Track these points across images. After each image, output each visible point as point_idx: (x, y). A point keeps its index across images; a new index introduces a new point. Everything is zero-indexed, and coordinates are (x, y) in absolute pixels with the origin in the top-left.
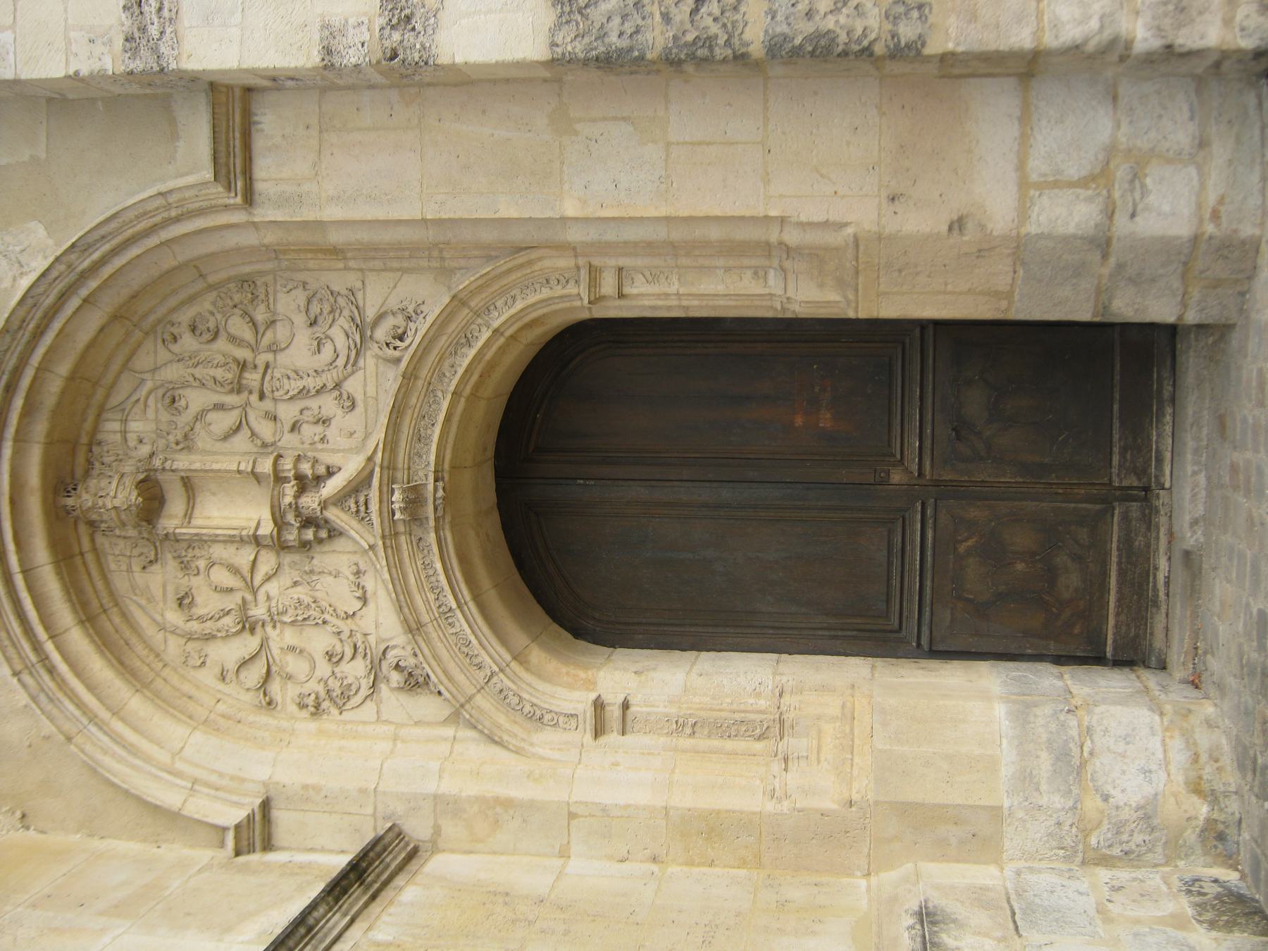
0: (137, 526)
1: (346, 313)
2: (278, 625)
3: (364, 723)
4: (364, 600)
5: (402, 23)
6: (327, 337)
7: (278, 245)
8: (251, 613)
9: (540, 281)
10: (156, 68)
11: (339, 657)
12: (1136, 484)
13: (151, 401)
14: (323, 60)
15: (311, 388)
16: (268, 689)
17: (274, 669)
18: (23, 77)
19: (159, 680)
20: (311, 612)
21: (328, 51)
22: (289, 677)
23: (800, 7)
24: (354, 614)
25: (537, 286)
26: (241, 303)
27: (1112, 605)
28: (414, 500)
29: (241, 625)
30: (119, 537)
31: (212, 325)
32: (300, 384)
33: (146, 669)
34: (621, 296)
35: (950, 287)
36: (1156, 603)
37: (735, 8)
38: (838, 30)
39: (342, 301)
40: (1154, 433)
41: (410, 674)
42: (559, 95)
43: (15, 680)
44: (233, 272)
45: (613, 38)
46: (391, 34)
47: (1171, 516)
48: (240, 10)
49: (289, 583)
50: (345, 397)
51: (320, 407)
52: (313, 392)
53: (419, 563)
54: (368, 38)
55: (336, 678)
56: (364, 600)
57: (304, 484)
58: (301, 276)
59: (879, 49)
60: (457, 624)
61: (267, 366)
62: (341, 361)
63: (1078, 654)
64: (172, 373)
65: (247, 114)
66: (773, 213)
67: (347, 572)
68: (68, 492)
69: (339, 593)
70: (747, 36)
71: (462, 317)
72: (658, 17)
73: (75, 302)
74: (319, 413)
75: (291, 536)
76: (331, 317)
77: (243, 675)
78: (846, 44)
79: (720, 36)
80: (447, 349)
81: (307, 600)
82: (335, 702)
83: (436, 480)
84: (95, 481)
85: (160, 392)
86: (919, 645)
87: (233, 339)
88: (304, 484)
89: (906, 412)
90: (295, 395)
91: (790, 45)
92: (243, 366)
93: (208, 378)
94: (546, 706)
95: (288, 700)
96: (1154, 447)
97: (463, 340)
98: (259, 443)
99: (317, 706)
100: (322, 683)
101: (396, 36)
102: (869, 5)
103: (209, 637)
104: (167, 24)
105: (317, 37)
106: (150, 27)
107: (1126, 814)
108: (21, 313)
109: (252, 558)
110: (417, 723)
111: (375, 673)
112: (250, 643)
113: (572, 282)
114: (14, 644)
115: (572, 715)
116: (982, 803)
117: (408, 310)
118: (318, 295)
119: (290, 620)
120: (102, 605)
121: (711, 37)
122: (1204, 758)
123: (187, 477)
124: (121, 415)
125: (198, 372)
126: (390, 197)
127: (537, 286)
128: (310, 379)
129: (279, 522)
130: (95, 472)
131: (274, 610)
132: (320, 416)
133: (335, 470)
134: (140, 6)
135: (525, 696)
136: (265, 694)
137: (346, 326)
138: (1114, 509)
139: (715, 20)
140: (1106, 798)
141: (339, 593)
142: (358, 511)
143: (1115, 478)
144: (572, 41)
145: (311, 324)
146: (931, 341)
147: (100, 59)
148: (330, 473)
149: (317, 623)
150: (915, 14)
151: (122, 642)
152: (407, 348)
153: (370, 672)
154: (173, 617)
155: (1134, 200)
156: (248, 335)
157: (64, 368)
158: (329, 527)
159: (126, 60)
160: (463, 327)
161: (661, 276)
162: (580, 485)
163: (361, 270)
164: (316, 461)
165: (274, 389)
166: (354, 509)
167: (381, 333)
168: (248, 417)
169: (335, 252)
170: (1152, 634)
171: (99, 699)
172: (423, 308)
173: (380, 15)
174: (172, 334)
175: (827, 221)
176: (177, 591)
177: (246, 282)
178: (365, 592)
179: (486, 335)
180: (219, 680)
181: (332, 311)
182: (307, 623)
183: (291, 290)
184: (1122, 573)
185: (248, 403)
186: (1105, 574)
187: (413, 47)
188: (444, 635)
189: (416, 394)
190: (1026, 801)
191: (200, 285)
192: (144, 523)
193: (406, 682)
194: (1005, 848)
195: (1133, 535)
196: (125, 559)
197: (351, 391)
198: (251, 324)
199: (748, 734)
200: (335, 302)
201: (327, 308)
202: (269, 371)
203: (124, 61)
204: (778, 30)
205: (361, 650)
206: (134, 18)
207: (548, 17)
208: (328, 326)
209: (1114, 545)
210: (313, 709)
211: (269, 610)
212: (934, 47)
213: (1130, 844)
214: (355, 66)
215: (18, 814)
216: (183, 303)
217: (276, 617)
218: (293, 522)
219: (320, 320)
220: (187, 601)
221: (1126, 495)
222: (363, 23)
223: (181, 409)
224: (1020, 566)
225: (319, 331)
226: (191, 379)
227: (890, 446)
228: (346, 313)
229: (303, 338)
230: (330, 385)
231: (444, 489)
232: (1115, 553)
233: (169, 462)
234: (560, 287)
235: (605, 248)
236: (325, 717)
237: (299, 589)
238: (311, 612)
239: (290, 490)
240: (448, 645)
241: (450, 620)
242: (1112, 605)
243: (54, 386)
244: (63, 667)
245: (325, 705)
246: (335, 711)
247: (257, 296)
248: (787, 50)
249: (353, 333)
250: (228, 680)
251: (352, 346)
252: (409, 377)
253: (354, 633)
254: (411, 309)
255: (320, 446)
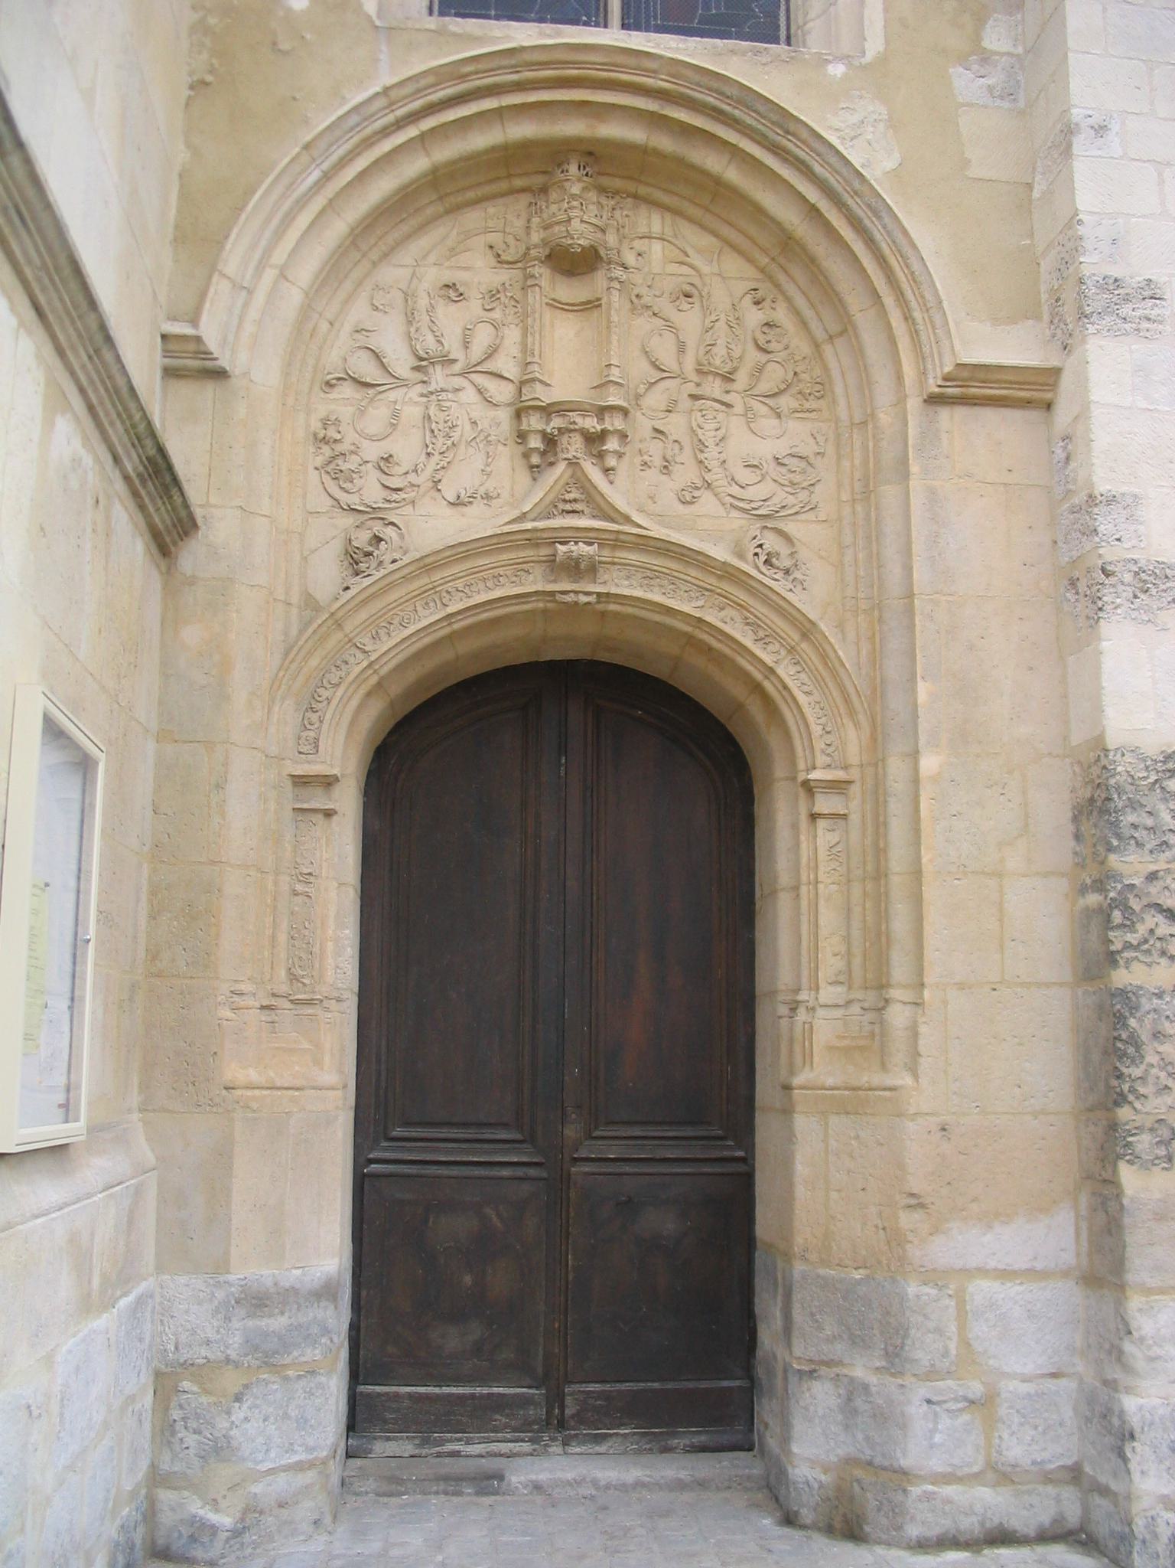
0: (545, 242)
1: (791, 500)
2: (425, 399)
3: (304, 497)
4: (458, 503)
5: (1141, 584)
6: (763, 477)
7: (875, 427)
8: (438, 368)
9: (830, 724)
10: (1088, 310)
11: (386, 470)
12: (568, 1412)
13: (685, 269)
14: (1102, 495)
15: (706, 455)
16: (345, 383)
17: (371, 391)
18: (1076, 164)
19: (358, 256)
20: (441, 440)
21: (1112, 500)
22: (362, 412)
23: (1167, 1024)
24: (439, 490)
25: (823, 720)
26: (799, 381)
27: (422, 1390)
28: (575, 568)
29: (426, 356)
30: (529, 221)
31: (773, 346)
32: (710, 442)
33: (372, 241)
34: (814, 817)
35: (834, 1195)
36: (425, 1442)
37: (1163, 953)
38: (1143, 1067)
39: (803, 495)
40: (626, 1431)
41: (369, 554)
42: (1050, 754)
43: (378, 89)
44: (835, 373)
45: (1131, 818)
46: (1130, 571)
47: (532, 1455)
48: (1149, 407)
49: (475, 415)
50: (696, 493)
51: (682, 464)
52: (701, 456)
53: (501, 571)
54: (1126, 546)
55: (360, 465)
56: (458, 503)
57: (594, 440)
58: (830, 450)
59: (1124, 1113)
60: (427, 612)
61: (728, 406)
62: (735, 490)
63: (361, 1352)
64: (720, 296)
65: (1027, 404)
66: (926, 993)
67: (490, 485)
68: (584, 168)
69: (463, 477)
70: (1136, 966)
71: (790, 633)
72: (1153, 868)
73: (812, 195)
74: (676, 463)
75: (534, 422)
76: (786, 483)
77: (365, 355)
78: (1130, 1076)
79: (1134, 935)
80: (752, 613)
81: (456, 435)
82: (330, 462)
83: (599, 594)
84: (595, 199)
85: (696, 281)
86: (371, 1161)
87: (760, 369)
88: (594, 440)
89: (694, 1143)
90: (697, 435)
91: (1127, 1014)
92: (728, 378)
93: (715, 337)
94: (328, 716)
95: (333, 407)
96: (611, 1432)
97: (761, 634)
98: (642, 389)
99: (325, 440)
100: (353, 448)
101: (1128, 577)
102: (1169, 1100)
103: (410, 319)
104: (1134, 325)
105: (1124, 489)
106: (1130, 306)
107: (222, 1424)
108: (805, 134)
109: (506, 375)
110: (305, 559)
111: (367, 512)
112: (401, 362)
113: (828, 760)
114: (419, 91)
115: (317, 747)
116: (233, 1249)
117: (796, 572)
118: (809, 469)
119: (432, 414)
120: (447, 195)
121: (1134, 926)
122: (284, 1513)
123: (600, 306)
124: (670, 234)
125: (721, 325)
126: (937, 558)
127: (823, 720)
128: (715, 454)
129: (548, 411)
130: (604, 200)
131: (443, 395)
132: (673, 463)
133: (611, 477)
134: (1151, 298)
135: (340, 692)
136: (339, 379)
137: (775, 500)
138: (537, 1388)
139: (1152, 931)
140: (238, 1398)
141: (463, 477)
142: (565, 501)
143: (576, 1387)
144: (1128, 772)
145: (778, 459)
146: (725, 1170)
147: (1095, 249)
148: (607, 471)
149: (427, 446)
150: (1162, 1151)
151: (405, 216)
152: (757, 568)
153: (368, 506)
154: (432, 276)
155: (945, 1402)
156: (764, 386)
157: (733, 175)
158: (542, 467)
159: (1095, 278)
160: (777, 633)
161: (838, 864)
162: (560, 761)
163: (840, 519)
164: (620, 455)
165: (704, 412)
166: (568, 497)
167: (771, 542)
168: (670, 380)
169: (867, 493)
170: (388, 1439)
171: (350, 184)
172: (799, 587)
173: (1149, 561)
174: (763, 300)
175: (920, 1055)
176: (465, 284)
177: (822, 389)
178: (464, 505)
179: (768, 659)
180: (356, 326)
181: (793, 484)
182: (428, 433)
183: (815, 438)
184: (461, 1399)
185: (685, 381)
186: (457, 1380)
187: (1118, 596)
188: (415, 597)
189: (700, 576)
190: (236, 1302)
191: (820, 335)
192: (547, 252)
193: (358, 548)
194: (176, 1277)
195: (507, 1411)
196: (502, 225)
197: (702, 500)
198: (777, 390)
199: (296, 960)
200: (803, 488)
201: (797, 478)
202: (723, 408)
203: (1094, 275)
204: (1143, 1000)
205: (395, 496)
206: (1139, 291)
207: (1152, 746)
208: (776, 478)
209: (495, 1390)
210: (321, 435)
211: (443, 390)
212: (1127, 1175)
213: (183, 1430)
214: (1095, 530)
215: (209, 78)
216: (797, 313)
217: (434, 397)
218: (552, 424)
219: (783, 470)
220: (452, 294)
221: (556, 1398)
222: (1141, 541)
223: (677, 303)
224: (468, 1279)
225: (771, 468)
226: (714, 318)
227: (608, 1123)
228: (791, 500)
229: (765, 449)
230: (708, 477)
231: (589, 603)
232: (485, 1391)
233: (618, 287)
234: (823, 746)
235: (878, 795)
236: (312, 449)
237: (468, 427)
238: (441, 440)
239: (591, 424)
240: (402, 600)
241: (432, 604)
242: (422, 1390)
243: (712, 162)
244: (387, 145)
245: (326, 451)
246: (319, 461)
247: (807, 400)
248: (1122, 1011)
249: (768, 506)
250: (357, 336)
251: (753, 505)
252: (728, 573)
253: (416, 488)
254: (797, 575)
255: (638, 460)
